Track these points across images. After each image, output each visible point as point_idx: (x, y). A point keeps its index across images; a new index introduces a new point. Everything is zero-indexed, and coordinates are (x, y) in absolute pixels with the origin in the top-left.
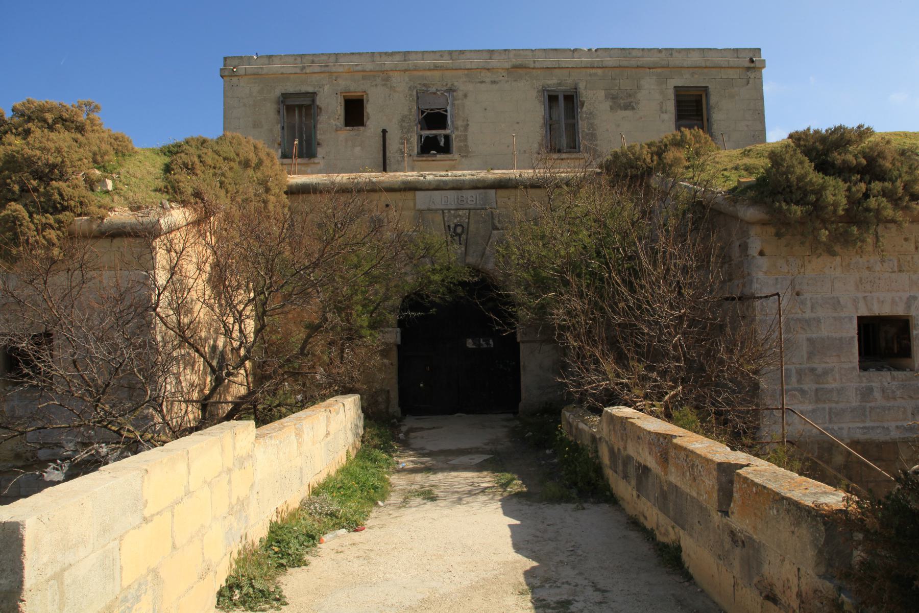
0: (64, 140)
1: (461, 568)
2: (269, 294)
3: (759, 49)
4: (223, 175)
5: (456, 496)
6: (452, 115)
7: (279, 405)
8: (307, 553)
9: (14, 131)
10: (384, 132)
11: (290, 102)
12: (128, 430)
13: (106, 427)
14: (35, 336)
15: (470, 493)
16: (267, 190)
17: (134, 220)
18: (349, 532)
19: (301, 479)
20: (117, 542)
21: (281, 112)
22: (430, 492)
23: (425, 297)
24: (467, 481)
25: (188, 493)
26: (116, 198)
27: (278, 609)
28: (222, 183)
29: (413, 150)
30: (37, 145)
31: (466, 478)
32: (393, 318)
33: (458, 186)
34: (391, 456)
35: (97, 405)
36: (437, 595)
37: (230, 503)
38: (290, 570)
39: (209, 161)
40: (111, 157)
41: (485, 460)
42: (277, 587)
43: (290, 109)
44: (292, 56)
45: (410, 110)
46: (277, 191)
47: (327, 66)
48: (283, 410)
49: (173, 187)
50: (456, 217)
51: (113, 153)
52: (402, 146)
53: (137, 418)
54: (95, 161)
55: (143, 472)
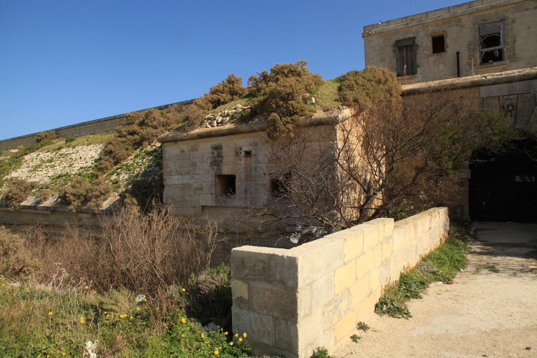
0: (293, 81)
1: (519, 315)
2: (395, 152)
4: (368, 89)
5: (512, 271)
6: (504, 36)
7: (401, 211)
8: (421, 292)
9: (272, 80)
10: (458, 53)
11: (401, 45)
12: (326, 220)
13: (316, 218)
14: (285, 174)
15: (522, 271)
16: (391, 95)
17: (326, 116)
18: (444, 284)
19: (416, 251)
20: (333, 272)
21: (396, 51)
22: (493, 267)
23: (488, 150)
24: (519, 263)
25: (363, 253)
26: (317, 106)
27: (407, 319)
28: (367, 93)
29: (477, 62)
30: (282, 85)
31: (518, 262)
32: (467, 163)
33: (509, 80)
34: (466, 244)
35: (312, 207)
36: (503, 328)
37: (382, 260)
38: (412, 300)
39: (360, 83)
40: (313, 86)
41: (530, 252)
42: (406, 307)
43: (400, 49)
44: (400, 19)
45: (474, 37)
46: (396, 95)
47: (421, 20)
48: (403, 214)
49: (343, 98)
50: (508, 100)
51: (314, 84)
52: (469, 61)
53: (330, 215)
54: (306, 89)
55: (344, 240)
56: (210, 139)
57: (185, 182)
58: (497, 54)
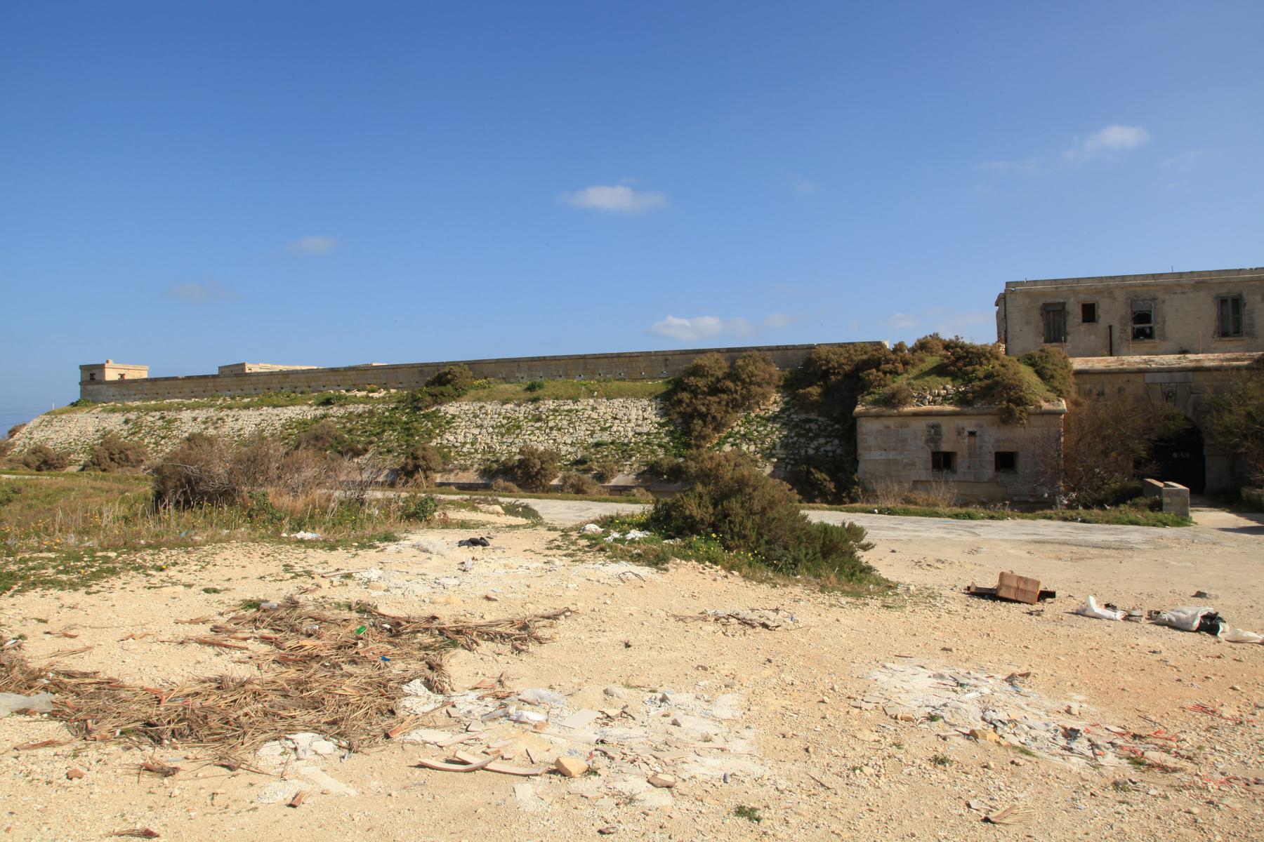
10: (1110, 327)
11: (1048, 309)
43: (1048, 312)
56: (926, 418)
57: (891, 458)
58: (1148, 331)
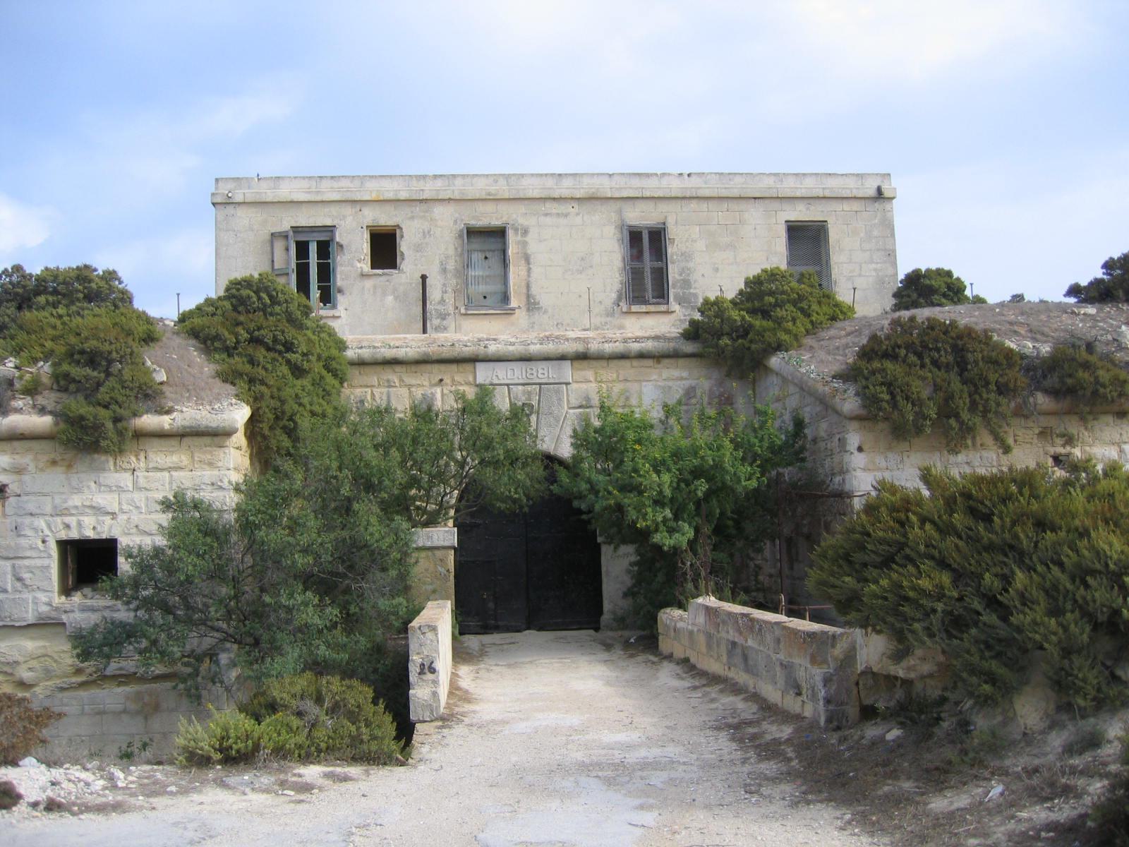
3: (889, 175)
10: (424, 278)
